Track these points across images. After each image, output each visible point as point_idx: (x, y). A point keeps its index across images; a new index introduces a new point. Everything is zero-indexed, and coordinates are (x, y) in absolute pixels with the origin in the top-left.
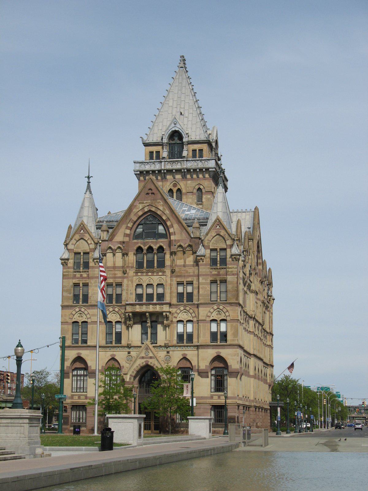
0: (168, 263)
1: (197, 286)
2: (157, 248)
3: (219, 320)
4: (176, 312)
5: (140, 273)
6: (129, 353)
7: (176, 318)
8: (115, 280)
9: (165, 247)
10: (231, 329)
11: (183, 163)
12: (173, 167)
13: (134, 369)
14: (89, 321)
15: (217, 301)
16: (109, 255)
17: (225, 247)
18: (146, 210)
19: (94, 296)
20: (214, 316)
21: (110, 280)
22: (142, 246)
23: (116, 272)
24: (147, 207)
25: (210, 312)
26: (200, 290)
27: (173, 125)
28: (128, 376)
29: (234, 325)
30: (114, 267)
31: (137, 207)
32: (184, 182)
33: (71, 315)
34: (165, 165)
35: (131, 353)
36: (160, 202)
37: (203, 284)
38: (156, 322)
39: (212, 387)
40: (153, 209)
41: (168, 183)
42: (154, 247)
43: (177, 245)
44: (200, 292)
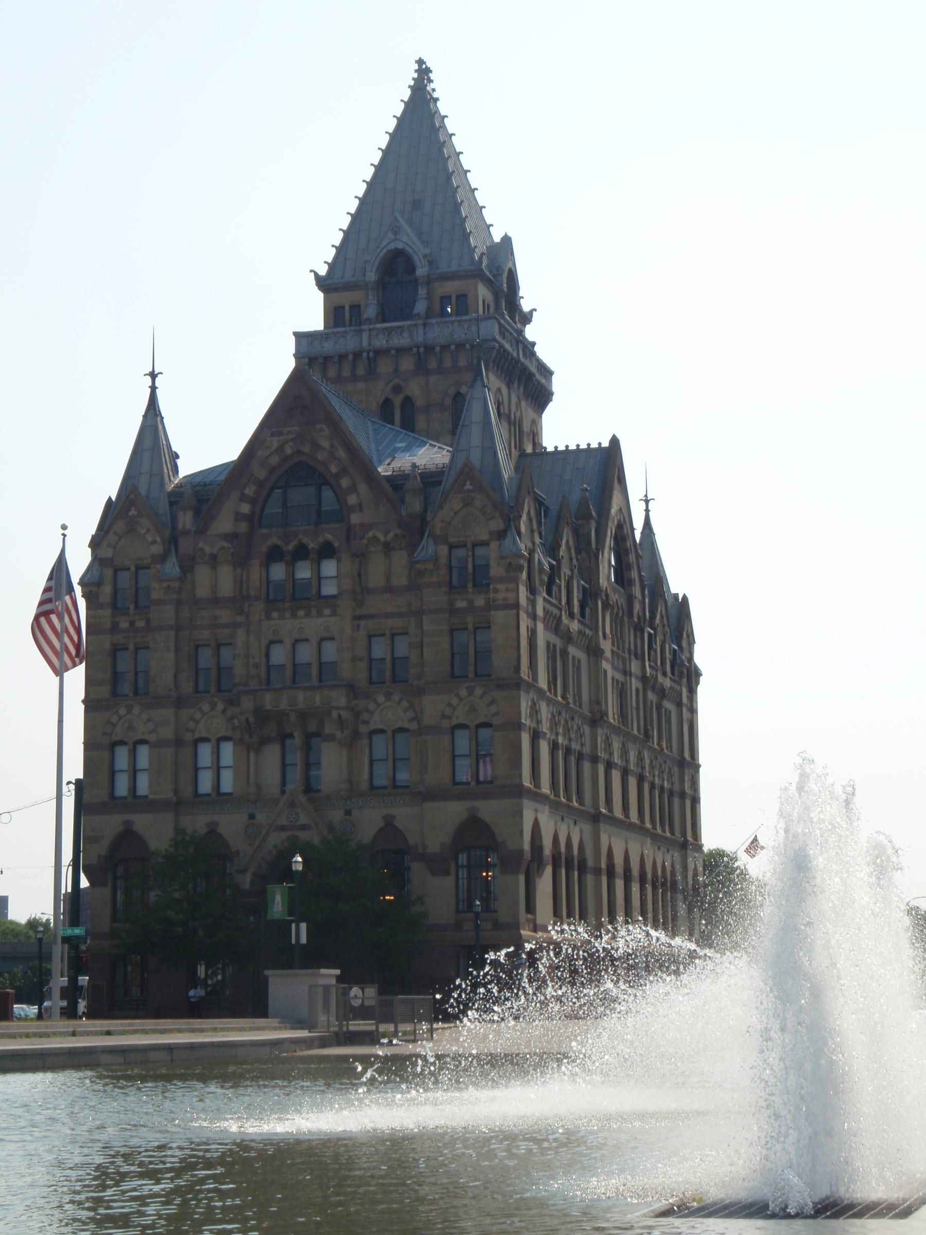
3: (472, 725)
6: (252, 817)
7: (366, 723)
9: (336, 544)
11: (415, 332)
12: (391, 342)
17: (485, 537)
18: (288, 451)
20: (460, 716)
25: (449, 705)
26: (426, 649)
27: (391, 235)
28: (248, 877)
30: (216, 601)
34: (370, 340)
38: (317, 734)
39: (461, 897)
40: (306, 449)
42: (311, 545)
44: (425, 657)
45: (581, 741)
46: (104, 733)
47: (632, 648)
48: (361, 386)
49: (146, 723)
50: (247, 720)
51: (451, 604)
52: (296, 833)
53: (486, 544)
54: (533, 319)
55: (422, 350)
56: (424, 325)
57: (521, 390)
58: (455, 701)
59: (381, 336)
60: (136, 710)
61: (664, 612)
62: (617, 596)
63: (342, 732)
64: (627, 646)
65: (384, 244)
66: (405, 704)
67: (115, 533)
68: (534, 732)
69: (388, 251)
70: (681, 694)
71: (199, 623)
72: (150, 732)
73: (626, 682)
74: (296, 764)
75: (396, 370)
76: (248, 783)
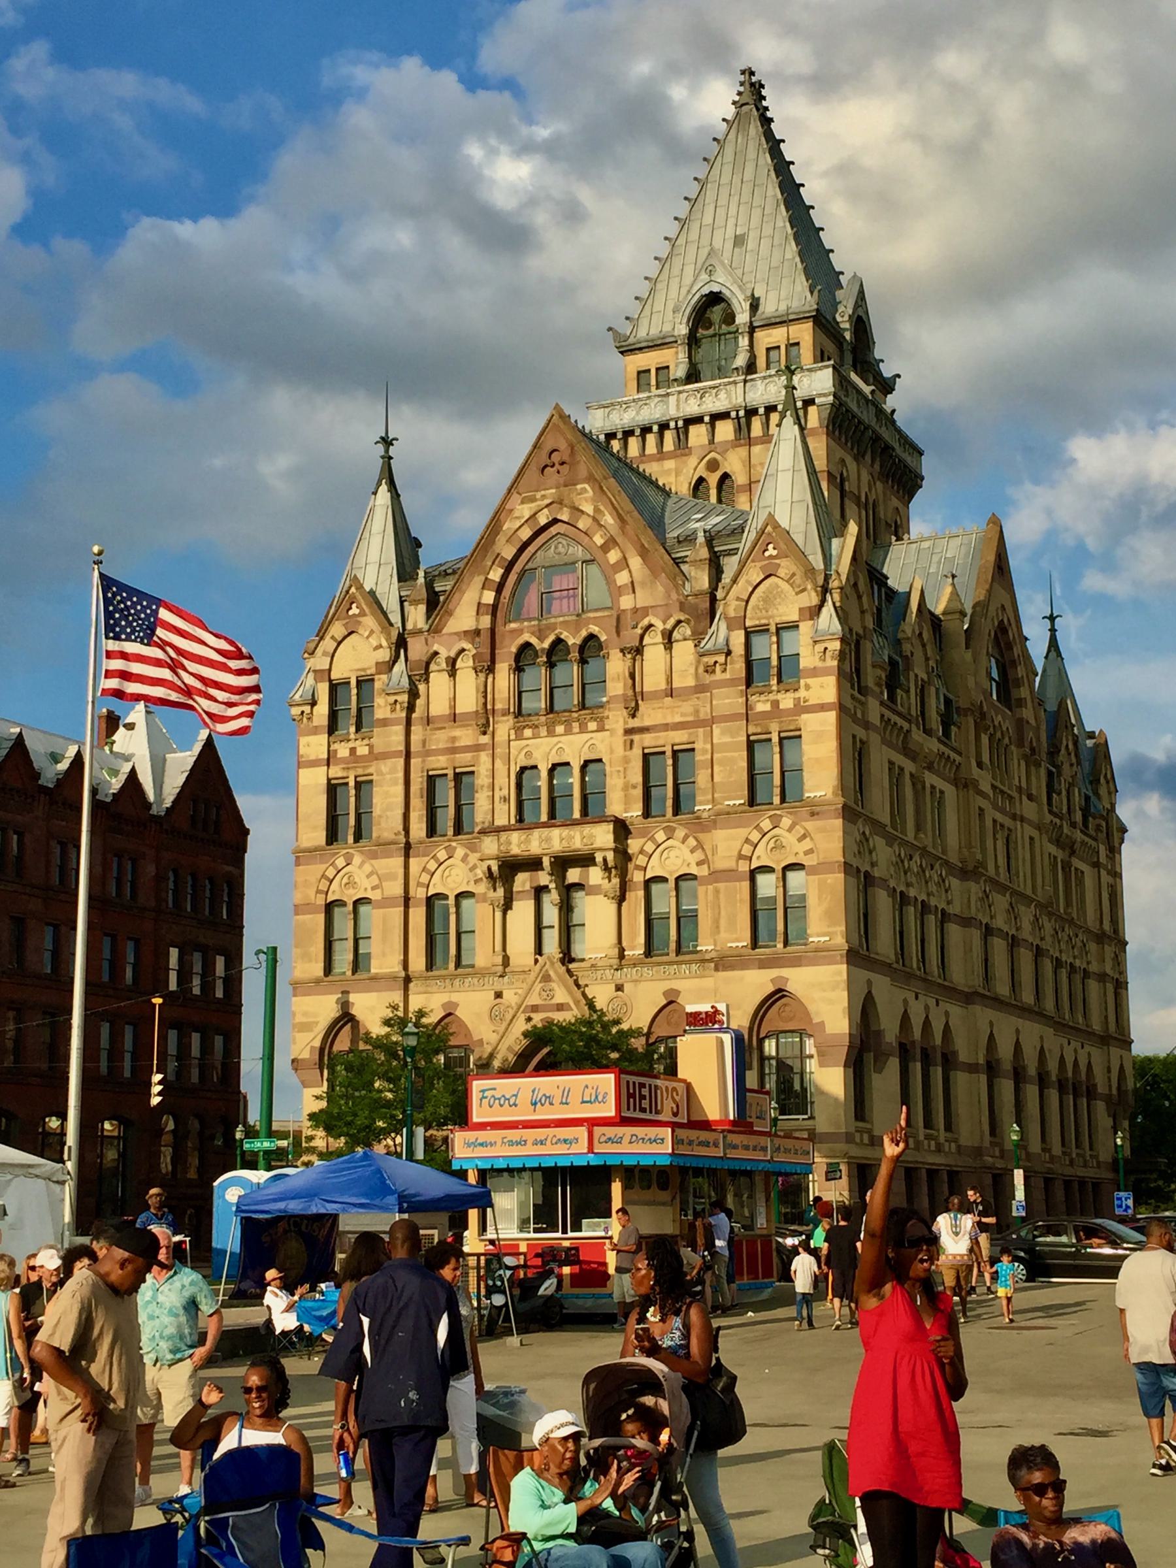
0: (616, 687)
1: (709, 757)
2: (579, 642)
3: (779, 868)
4: (642, 852)
6: (499, 995)
8: (453, 760)
9: (603, 638)
10: (820, 898)
13: (509, 1049)
17: (795, 617)
19: (388, 813)
22: (534, 641)
23: (457, 733)
24: (546, 511)
25: (747, 841)
27: (704, 277)
31: (516, 514)
32: (742, 452)
34: (678, 405)
36: (585, 490)
37: (726, 747)
41: (693, 461)
42: (571, 642)
46: (318, 891)
47: (1024, 785)
48: (670, 464)
49: (368, 876)
50: (489, 869)
51: (748, 707)
52: (550, 1015)
53: (794, 626)
55: (742, 413)
56: (745, 381)
57: (877, 467)
59: (692, 401)
60: (357, 860)
62: (1000, 718)
64: (1016, 782)
66: (692, 842)
67: (333, 637)
68: (865, 877)
69: (702, 296)
72: (373, 888)
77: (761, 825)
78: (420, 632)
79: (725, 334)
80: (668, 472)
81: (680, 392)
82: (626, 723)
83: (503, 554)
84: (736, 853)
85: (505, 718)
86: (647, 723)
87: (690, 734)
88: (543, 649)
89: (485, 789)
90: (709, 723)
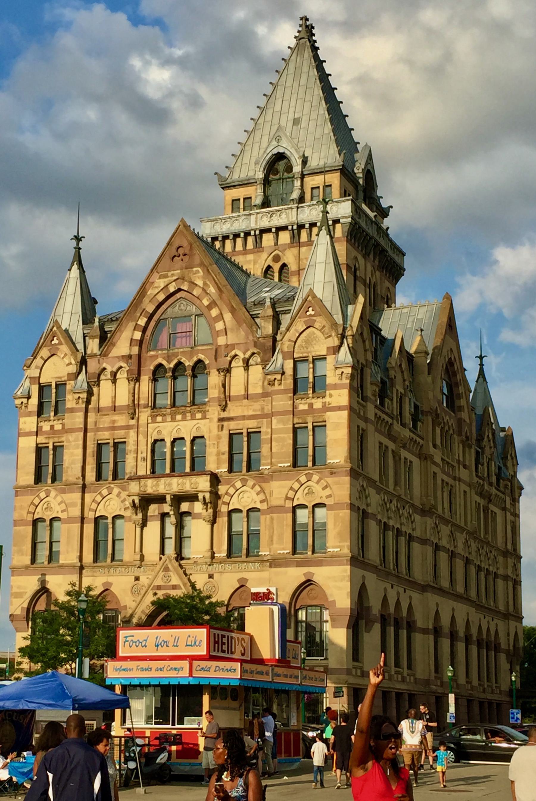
0: (214, 392)
1: (270, 436)
3: (310, 505)
4: (227, 493)
5: (161, 416)
6: (137, 579)
8: (113, 434)
9: (207, 362)
14: (63, 516)
15: (307, 466)
16: (106, 385)
19: (73, 466)
21: (104, 434)
22: (164, 363)
23: (116, 418)
24: (174, 283)
25: (291, 488)
27: (275, 143)
29: (341, 514)
31: (156, 285)
32: (295, 250)
33: (32, 505)
34: (256, 221)
35: (140, 580)
37: (279, 431)
41: (264, 255)
43: (229, 355)
44: (274, 450)
45: (412, 526)
46: (29, 512)
47: (461, 459)
48: (250, 257)
49: (59, 504)
54: (390, 214)
56: (298, 208)
57: (377, 262)
58: (296, 486)
61: (490, 436)
63: (207, 511)
65: (269, 150)
66: (257, 488)
67: (42, 357)
69: (273, 155)
70: (505, 501)
71: (102, 426)
73: (456, 485)
74: (171, 538)
75: (276, 244)
76: (135, 552)
77: (300, 479)
78: (95, 355)
79: (286, 179)
80: (249, 262)
81: (258, 213)
82: (219, 414)
83: (147, 309)
84: (284, 496)
85: (146, 410)
86: (232, 415)
87: (258, 422)
88: (170, 368)
89: (132, 453)
90: (270, 416)
